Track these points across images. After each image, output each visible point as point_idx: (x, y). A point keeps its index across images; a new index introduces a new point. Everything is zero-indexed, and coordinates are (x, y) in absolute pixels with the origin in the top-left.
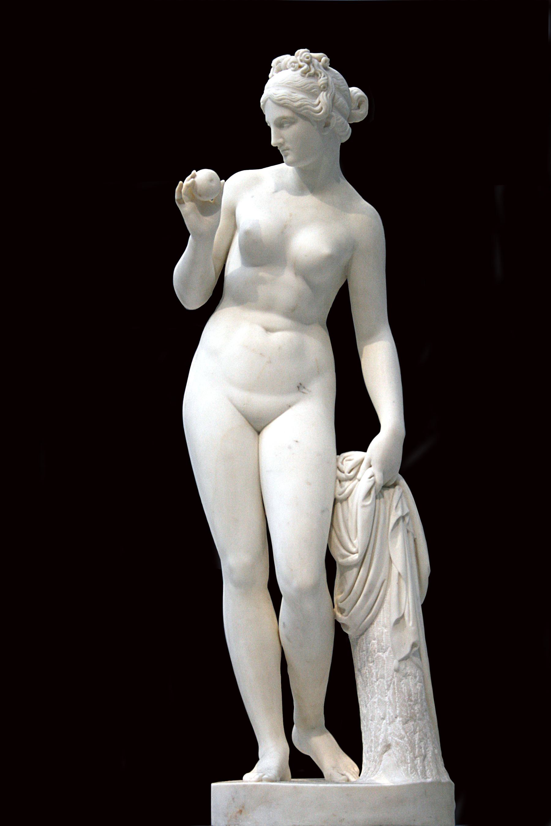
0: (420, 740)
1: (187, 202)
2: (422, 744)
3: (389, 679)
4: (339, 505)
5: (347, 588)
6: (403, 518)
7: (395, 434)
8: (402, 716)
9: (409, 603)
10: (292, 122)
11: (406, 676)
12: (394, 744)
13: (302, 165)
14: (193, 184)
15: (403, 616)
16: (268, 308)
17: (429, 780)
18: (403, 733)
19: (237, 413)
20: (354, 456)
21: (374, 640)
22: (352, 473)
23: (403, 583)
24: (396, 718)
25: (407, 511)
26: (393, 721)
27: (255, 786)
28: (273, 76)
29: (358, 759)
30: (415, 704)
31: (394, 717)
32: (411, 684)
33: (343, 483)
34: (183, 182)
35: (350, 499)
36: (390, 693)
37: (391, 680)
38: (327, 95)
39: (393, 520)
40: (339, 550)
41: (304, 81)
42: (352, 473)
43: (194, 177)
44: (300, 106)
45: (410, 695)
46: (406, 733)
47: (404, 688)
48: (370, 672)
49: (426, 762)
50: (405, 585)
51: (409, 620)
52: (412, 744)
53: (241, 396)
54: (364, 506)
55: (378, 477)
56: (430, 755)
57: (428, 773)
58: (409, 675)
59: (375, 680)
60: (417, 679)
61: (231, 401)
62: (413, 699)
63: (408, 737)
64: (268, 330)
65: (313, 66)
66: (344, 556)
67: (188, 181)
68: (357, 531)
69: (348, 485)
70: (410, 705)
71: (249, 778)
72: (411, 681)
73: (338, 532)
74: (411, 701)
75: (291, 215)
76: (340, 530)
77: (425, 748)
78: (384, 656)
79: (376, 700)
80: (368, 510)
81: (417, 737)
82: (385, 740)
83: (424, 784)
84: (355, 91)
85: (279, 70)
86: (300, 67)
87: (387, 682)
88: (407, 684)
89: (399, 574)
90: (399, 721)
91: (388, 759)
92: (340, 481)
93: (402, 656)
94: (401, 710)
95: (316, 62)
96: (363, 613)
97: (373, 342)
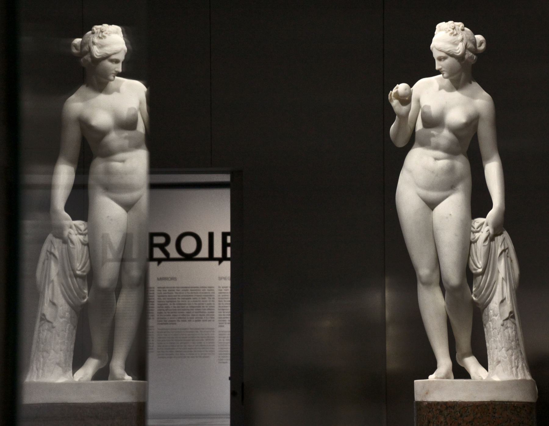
0: (515, 359)
1: (394, 100)
2: (516, 362)
3: (499, 329)
4: (473, 245)
5: (477, 285)
6: (504, 251)
7: (499, 210)
8: (505, 348)
9: (508, 293)
10: (445, 58)
11: (507, 328)
12: (502, 361)
13: (452, 78)
14: (397, 93)
15: (505, 299)
16: (436, 148)
17: (520, 378)
18: (506, 355)
19: (422, 201)
20: (480, 220)
21: (491, 310)
22: (479, 229)
23: (504, 283)
24: (503, 348)
25: (506, 247)
26: (501, 350)
27: (433, 381)
28: (437, 33)
29: (486, 368)
30: (512, 342)
31: (501, 348)
32: (510, 332)
33: (474, 234)
34: (392, 91)
35: (478, 242)
36: (499, 336)
37: (500, 330)
38: (462, 44)
39: (499, 251)
40: (473, 266)
41: (452, 38)
42: (479, 229)
43: (397, 88)
44: (449, 51)
45: (509, 337)
46: (508, 355)
47: (507, 334)
48: (490, 326)
49: (518, 369)
50: (506, 284)
51: (508, 300)
52: (511, 361)
53: (424, 193)
54: (484, 246)
55: (491, 231)
56: (520, 366)
57: (519, 375)
58: (509, 328)
59: (492, 330)
60: (513, 329)
61: (419, 195)
62: (511, 339)
63: (508, 357)
64: (436, 159)
65: (456, 30)
66: (475, 270)
67: (394, 90)
68: (481, 258)
69: (477, 235)
70: (509, 342)
71: (432, 377)
72: (510, 330)
73: (472, 258)
74: (510, 340)
75: (446, 102)
76: (473, 257)
77: (518, 363)
78: (496, 318)
79: (493, 340)
80: (486, 248)
81: (513, 357)
82: (497, 359)
83: (517, 380)
84: (479, 38)
85: (440, 30)
86: (449, 31)
87: (498, 331)
88: (508, 332)
89: (503, 278)
90: (504, 350)
91: (499, 368)
92: (473, 233)
93: (505, 318)
94: (505, 344)
95: (457, 27)
96: (485, 297)
97: (490, 162)
